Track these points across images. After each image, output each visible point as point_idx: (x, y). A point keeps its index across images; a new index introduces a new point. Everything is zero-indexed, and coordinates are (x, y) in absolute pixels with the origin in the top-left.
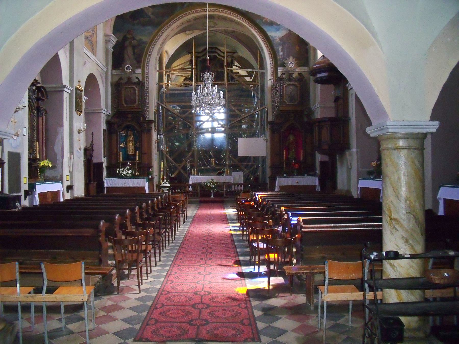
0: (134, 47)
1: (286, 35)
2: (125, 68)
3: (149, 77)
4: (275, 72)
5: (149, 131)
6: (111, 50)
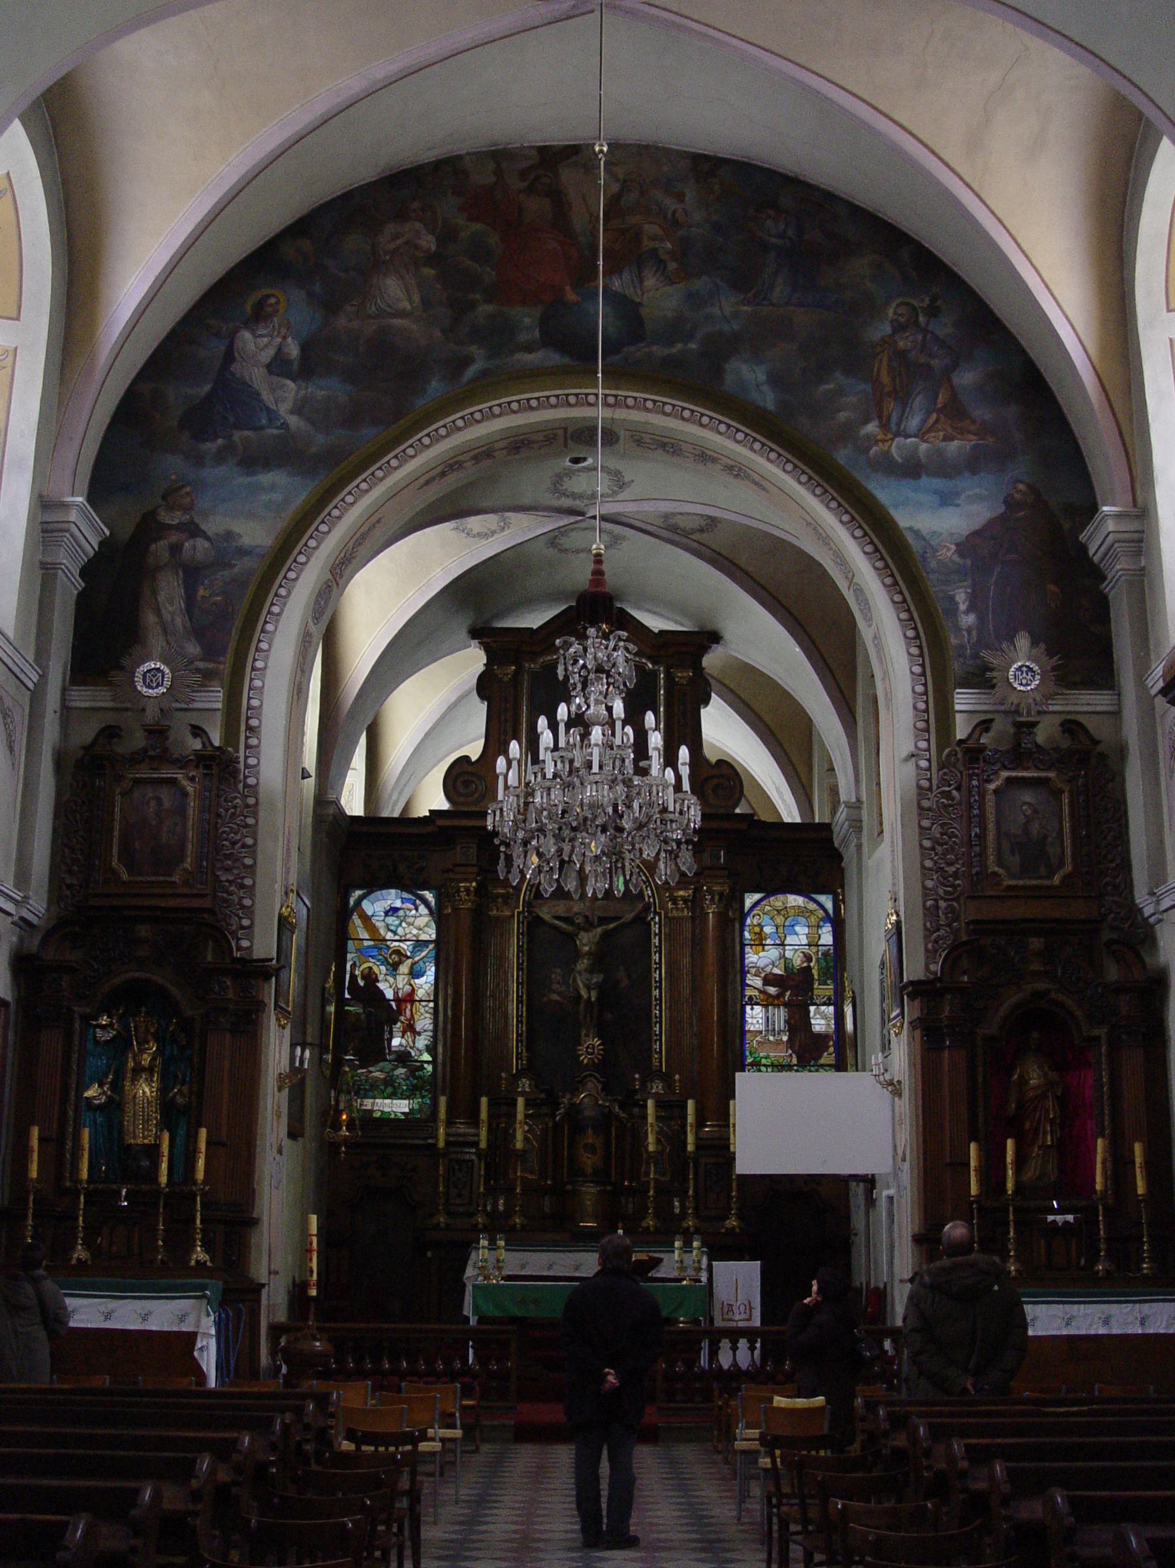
0: (192, 574)
1: (991, 523)
2: (138, 678)
3: (264, 731)
4: (938, 714)
5: (247, 1025)
6: (70, 585)
